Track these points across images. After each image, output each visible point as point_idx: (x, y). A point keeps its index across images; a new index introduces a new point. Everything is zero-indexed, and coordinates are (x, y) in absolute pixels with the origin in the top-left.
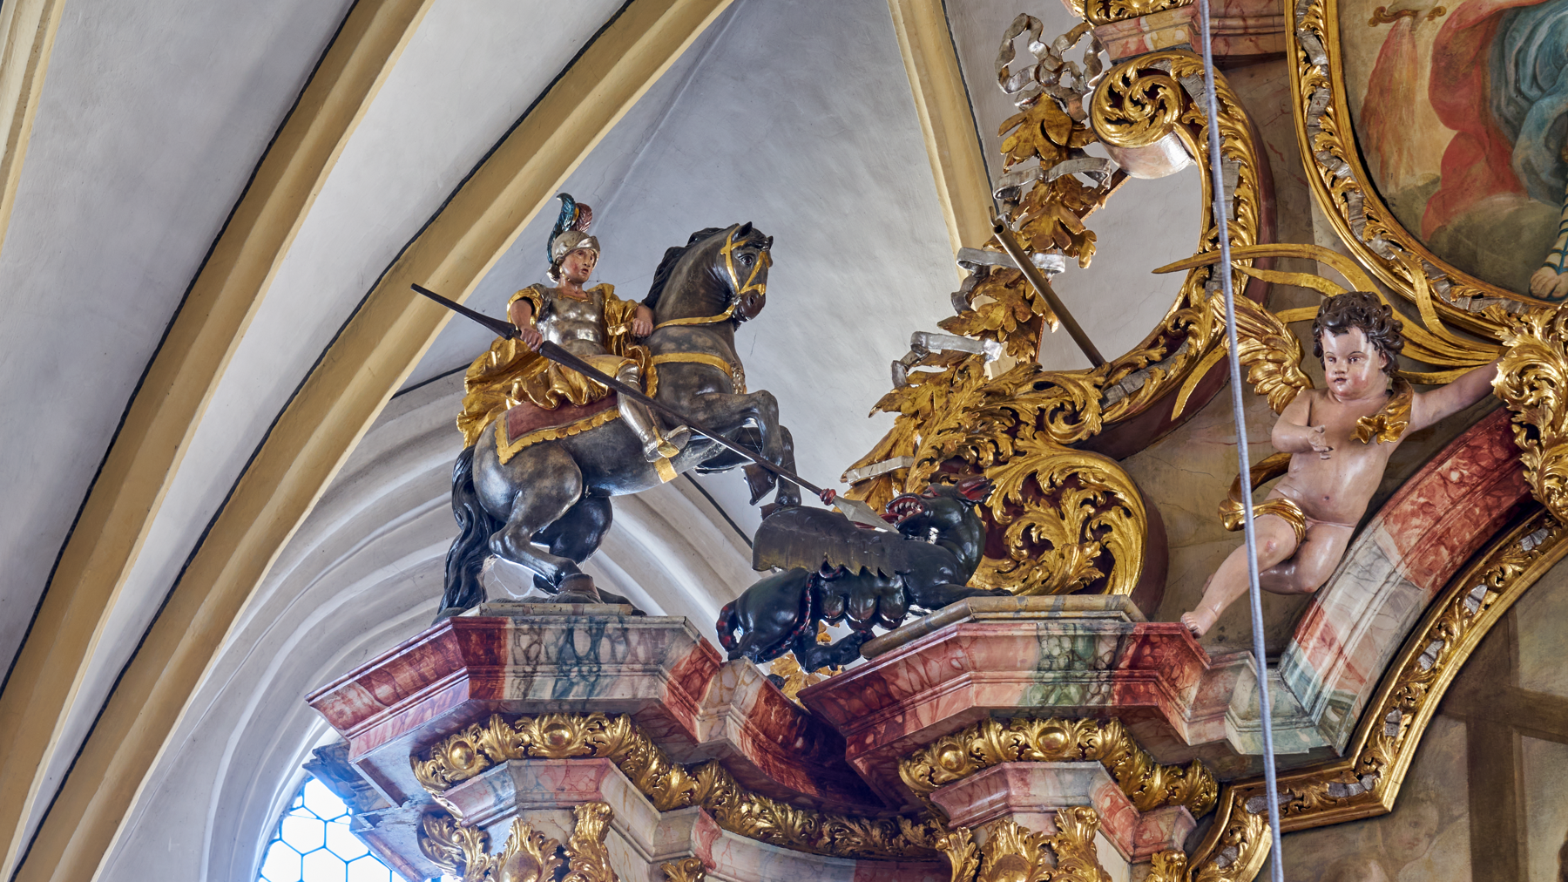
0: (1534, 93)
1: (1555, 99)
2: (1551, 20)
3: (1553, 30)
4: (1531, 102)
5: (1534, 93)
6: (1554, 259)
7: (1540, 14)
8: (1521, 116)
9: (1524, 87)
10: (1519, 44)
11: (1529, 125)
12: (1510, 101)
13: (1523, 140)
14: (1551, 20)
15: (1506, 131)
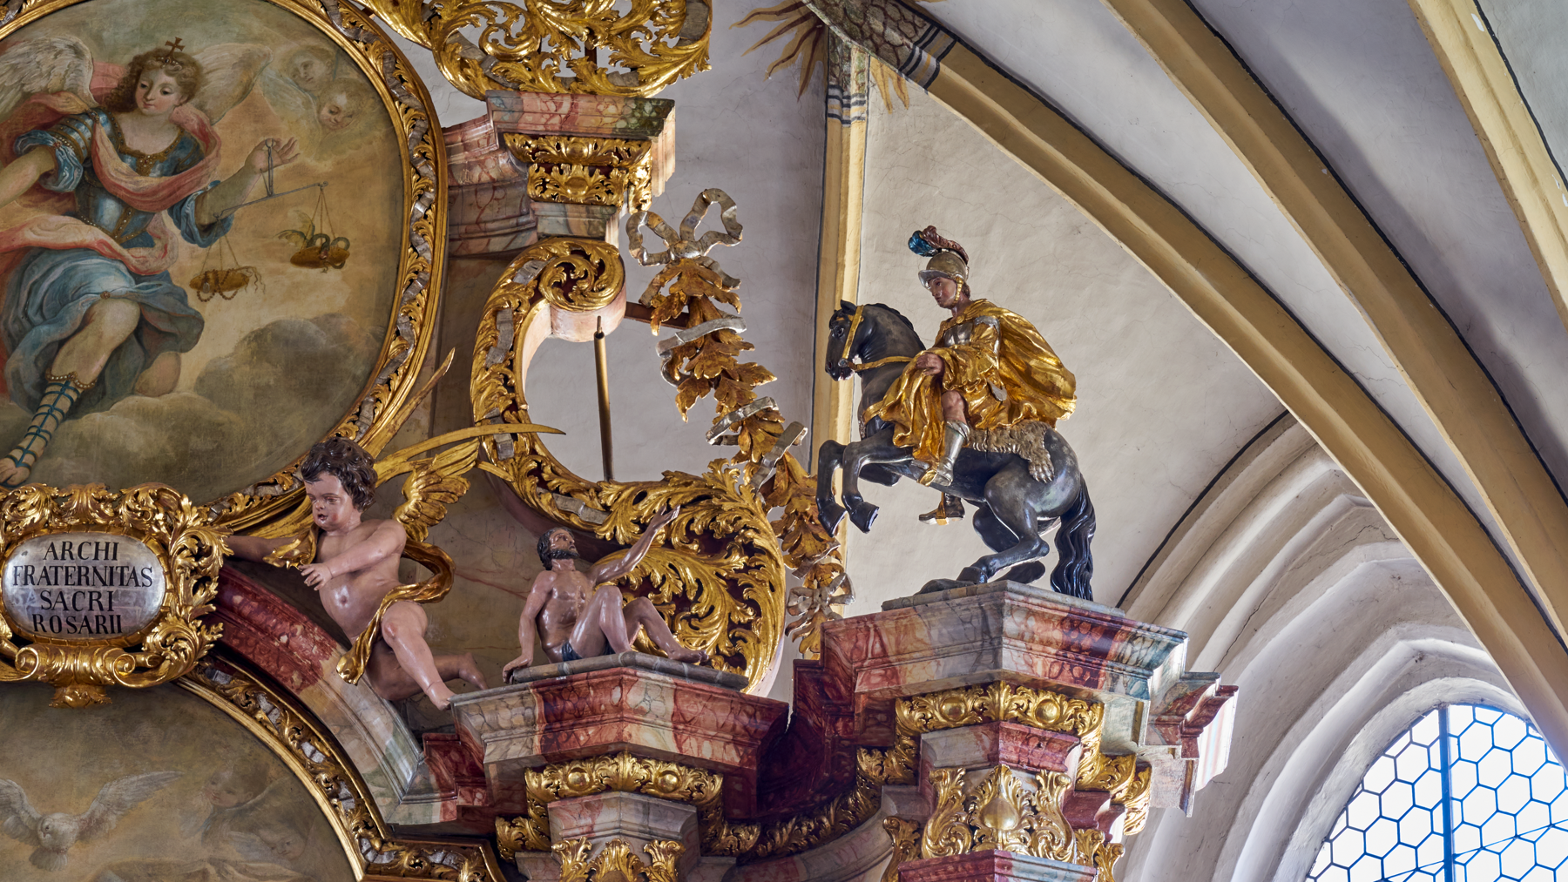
0: (37, 319)
1: (52, 328)
2: (67, 265)
3: (66, 274)
4: (33, 325)
5: (37, 319)
6: (17, 454)
7: (59, 258)
8: (22, 333)
9: (31, 312)
10: (36, 277)
11: (26, 343)
12: (16, 319)
13: (18, 354)
14: (67, 265)
15: (7, 343)
